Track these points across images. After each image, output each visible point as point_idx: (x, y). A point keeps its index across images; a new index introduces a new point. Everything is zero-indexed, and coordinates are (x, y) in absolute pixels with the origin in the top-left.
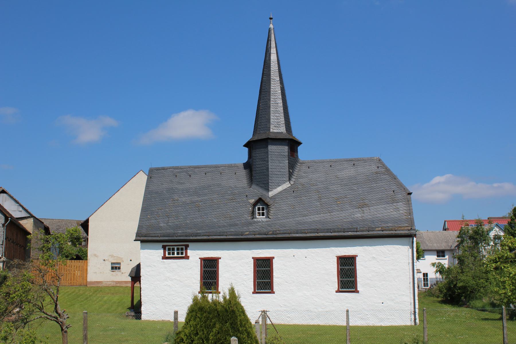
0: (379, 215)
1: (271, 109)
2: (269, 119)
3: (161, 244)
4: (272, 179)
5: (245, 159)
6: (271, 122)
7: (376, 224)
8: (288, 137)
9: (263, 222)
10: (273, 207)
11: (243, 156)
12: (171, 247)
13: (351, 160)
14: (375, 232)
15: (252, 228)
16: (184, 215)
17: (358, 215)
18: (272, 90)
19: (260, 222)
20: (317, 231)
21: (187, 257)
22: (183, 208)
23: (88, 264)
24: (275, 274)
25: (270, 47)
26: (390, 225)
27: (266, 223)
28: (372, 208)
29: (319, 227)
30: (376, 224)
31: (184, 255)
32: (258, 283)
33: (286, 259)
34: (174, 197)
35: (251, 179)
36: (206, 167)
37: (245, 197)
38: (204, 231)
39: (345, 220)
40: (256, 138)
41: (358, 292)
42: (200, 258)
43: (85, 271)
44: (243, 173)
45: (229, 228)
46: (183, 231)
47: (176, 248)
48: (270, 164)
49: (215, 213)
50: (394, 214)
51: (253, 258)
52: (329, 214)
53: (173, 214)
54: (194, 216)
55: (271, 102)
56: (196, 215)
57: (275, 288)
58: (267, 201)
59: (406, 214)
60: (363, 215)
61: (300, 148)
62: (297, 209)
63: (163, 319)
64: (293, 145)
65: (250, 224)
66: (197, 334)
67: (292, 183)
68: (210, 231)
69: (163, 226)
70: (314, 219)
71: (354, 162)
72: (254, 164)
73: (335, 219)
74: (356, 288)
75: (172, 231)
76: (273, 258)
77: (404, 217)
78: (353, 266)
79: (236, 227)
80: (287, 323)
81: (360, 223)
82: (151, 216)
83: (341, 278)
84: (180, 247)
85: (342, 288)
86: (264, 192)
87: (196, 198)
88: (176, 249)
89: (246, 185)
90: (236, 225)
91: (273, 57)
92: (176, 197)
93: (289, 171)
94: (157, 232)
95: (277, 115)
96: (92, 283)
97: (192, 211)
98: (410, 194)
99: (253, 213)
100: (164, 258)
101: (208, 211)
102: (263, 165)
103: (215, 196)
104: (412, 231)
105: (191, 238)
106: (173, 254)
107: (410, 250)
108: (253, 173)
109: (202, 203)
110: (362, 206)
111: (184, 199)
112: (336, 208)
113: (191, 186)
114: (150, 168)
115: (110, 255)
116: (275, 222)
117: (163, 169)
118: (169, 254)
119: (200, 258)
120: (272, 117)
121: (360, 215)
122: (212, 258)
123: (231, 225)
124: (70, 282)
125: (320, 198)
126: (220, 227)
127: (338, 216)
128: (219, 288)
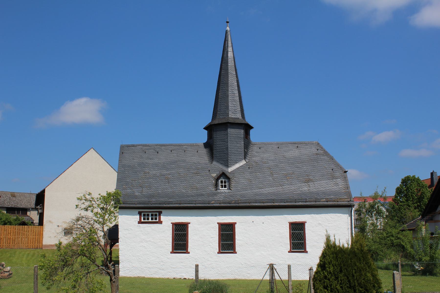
0: (322, 189)
1: (230, 98)
2: (227, 107)
3: (137, 211)
4: (231, 157)
5: (205, 139)
6: (230, 109)
7: (321, 196)
8: (243, 122)
9: (226, 193)
10: (233, 180)
11: (204, 137)
12: (146, 213)
13: (295, 143)
14: (321, 203)
15: (217, 198)
16: (156, 186)
17: (305, 189)
18: (229, 82)
19: (223, 193)
20: (273, 201)
21: (160, 222)
22: (154, 180)
23: (44, 229)
24: (237, 237)
25: (228, 46)
26: (332, 197)
27: (228, 194)
28: (316, 183)
29: (273, 197)
30: (321, 196)
31: (158, 220)
32: (222, 244)
33: (247, 226)
34: (146, 170)
35: (212, 156)
36: (171, 145)
37: (208, 171)
38: (175, 200)
39: (295, 192)
40: (216, 122)
41: (307, 252)
42: (171, 223)
43: (40, 235)
44: (204, 152)
45: (197, 197)
46: (156, 200)
47: (150, 214)
48: (229, 144)
49: (183, 184)
50: (335, 188)
51: (218, 223)
52: (281, 187)
53: (146, 185)
54: (165, 187)
55: (230, 92)
56: (167, 186)
57: (237, 249)
58: (228, 175)
59: (344, 188)
60: (309, 188)
61: (252, 131)
62: (253, 182)
63: (138, 275)
64: (247, 128)
65: (215, 194)
66: (341, 271)
67: (247, 161)
68: (181, 200)
69: (139, 194)
70: (268, 191)
71: (297, 145)
72: (215, 144)
73: (287, 191)
74: (305, 248)
75: (146, 199)
76: (236, 223)
77: (343, 191)
78: (302, 230)
79: (203, 197)
80: (247, 278)
81: (308, 195)
82: (127, 187)
83: (293, 240)
84: (154, 213)
85: (294, 249)
86: (224, 168)
87: (164, 172)
88: (150, 215)
89: (208, 161)
90: (202, 195)
91: (230, 54)
92: (147, 170)
93: (245, 151)
94: (134, 200)
95: (234, 103)
96: (46, 246)
97: (162, 183)
98: (346, 172)
99: (216, 185)
100: (140, 222)
101: (177, 183)
102: (223, 145)
103: (181, 170)
104: (351, 203)
105: (165, 205)
106: (148, 219)
107: (349, 218)
108: (214, 151)
109: (171, 176)
110: (308, 181)
111: (155, 172)
112: (287, 182)
113: (159, 161)
114: (121, 145)
115: (63, 222)
116: (236, 193)
117: (133, 146)
118: (144, 219)
119: (171, 223)
120: (230, 105)
121: (307, 189)
122: (182, 223)
123: (198, 195)
124: (27, 245)
125: (272, 174)
126: (188, 196)
127: (289, 189)
128: (189, 249)
